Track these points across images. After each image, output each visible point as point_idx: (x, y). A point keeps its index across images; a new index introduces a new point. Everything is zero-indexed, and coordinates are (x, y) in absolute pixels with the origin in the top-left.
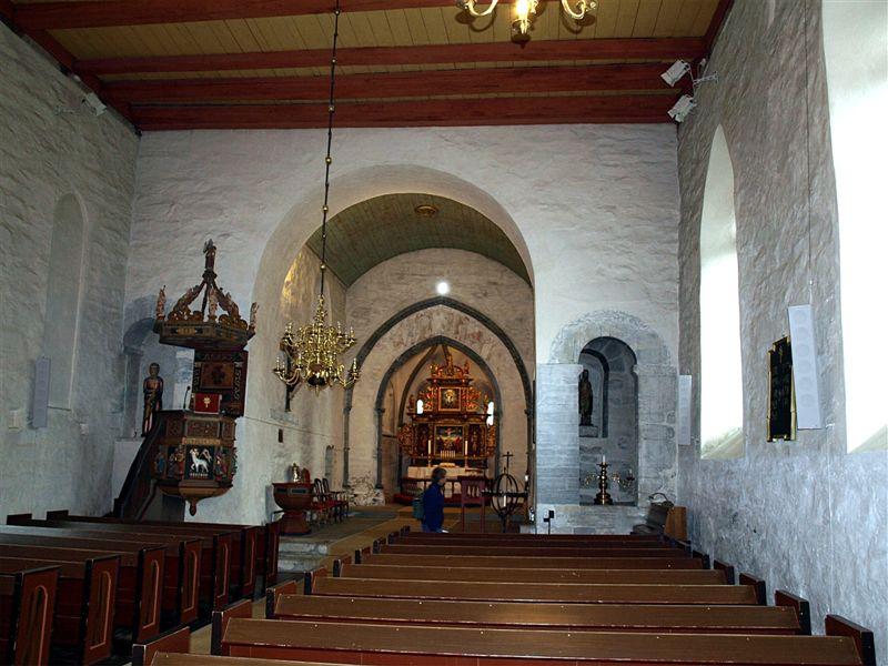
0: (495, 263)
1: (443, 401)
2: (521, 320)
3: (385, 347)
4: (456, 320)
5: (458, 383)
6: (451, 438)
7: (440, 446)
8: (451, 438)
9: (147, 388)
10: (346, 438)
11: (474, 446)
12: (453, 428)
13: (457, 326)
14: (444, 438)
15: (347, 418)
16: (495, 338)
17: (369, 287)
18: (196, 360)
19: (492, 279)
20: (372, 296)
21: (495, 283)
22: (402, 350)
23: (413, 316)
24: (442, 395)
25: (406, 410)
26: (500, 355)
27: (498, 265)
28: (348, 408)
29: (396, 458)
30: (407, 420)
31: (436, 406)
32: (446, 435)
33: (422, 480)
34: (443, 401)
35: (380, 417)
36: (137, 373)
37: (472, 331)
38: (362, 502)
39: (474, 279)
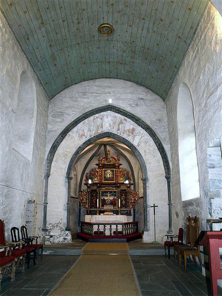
1: (105, 177)
2: (160, 120)
3: (73, 137)
4: (118, 121)
5: (114, 166)
6: (109, 198)
7: (104, 203)
8: (109, 198)
10: (46, 196)
11: (124, 202)
12: (111, 192)
14: (106, 198)
15: (47, 182)
16: (143, 131)
17: (64, 100)
19: (141, 96)
20: (66, 105)
21: (142, 99)
22: (84, 140)
23: (92, 118)
24: (104, 173)
25: (84, 182)
26: (146, 142)
27: (144, 88)
28: (48, 176)
29: (77, 210)
30: (84, 187)
31: (101, 179)
32: (107, 196)
33: (95, 224)
34: (105, 177)
35: (69, 183)
37: (128, 128)
38: (56, 241)
39: (130, 96)
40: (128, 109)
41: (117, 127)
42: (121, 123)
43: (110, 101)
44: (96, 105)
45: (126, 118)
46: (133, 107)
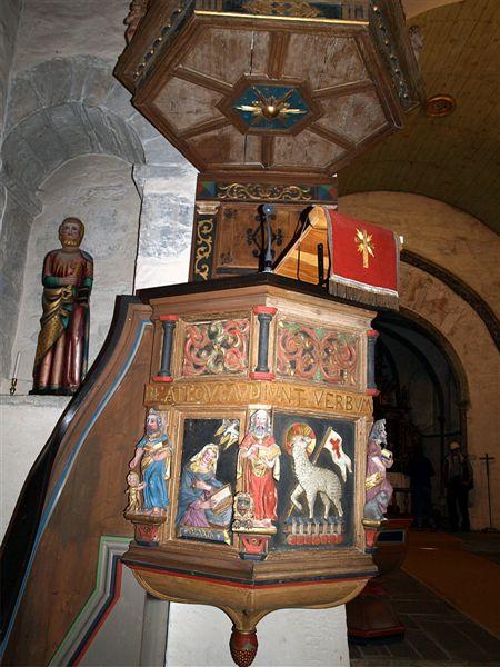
0: (462, 215)
9: (52, 269)
13: (414, 290)
18: (201, 195)
19: (461, 233)
21: (464, 239)
36: (23, 244)
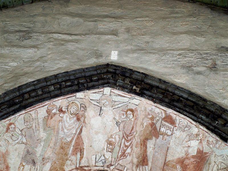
4: (141, 126)
23: (39, 111)
39: (185, 41)
40: (181, 79)
41: (137, 150)
42: (154, 131)
43: (114, 57)
44: (58, 65)
45: (170, 111)
46: (199, 73)
